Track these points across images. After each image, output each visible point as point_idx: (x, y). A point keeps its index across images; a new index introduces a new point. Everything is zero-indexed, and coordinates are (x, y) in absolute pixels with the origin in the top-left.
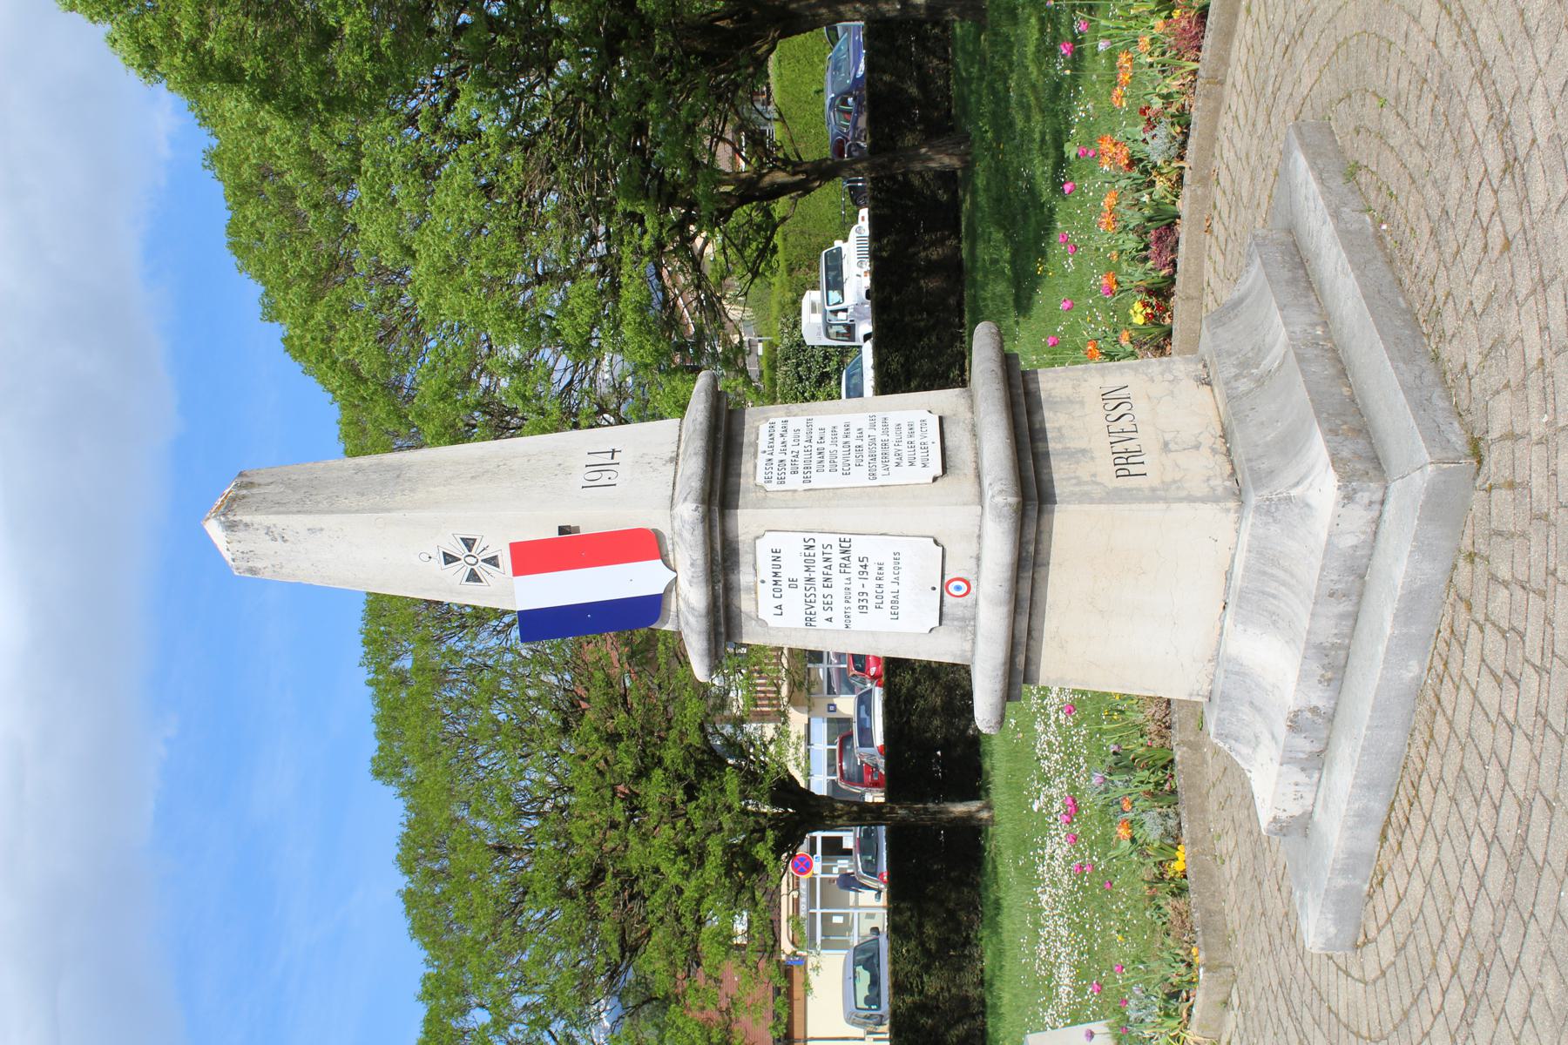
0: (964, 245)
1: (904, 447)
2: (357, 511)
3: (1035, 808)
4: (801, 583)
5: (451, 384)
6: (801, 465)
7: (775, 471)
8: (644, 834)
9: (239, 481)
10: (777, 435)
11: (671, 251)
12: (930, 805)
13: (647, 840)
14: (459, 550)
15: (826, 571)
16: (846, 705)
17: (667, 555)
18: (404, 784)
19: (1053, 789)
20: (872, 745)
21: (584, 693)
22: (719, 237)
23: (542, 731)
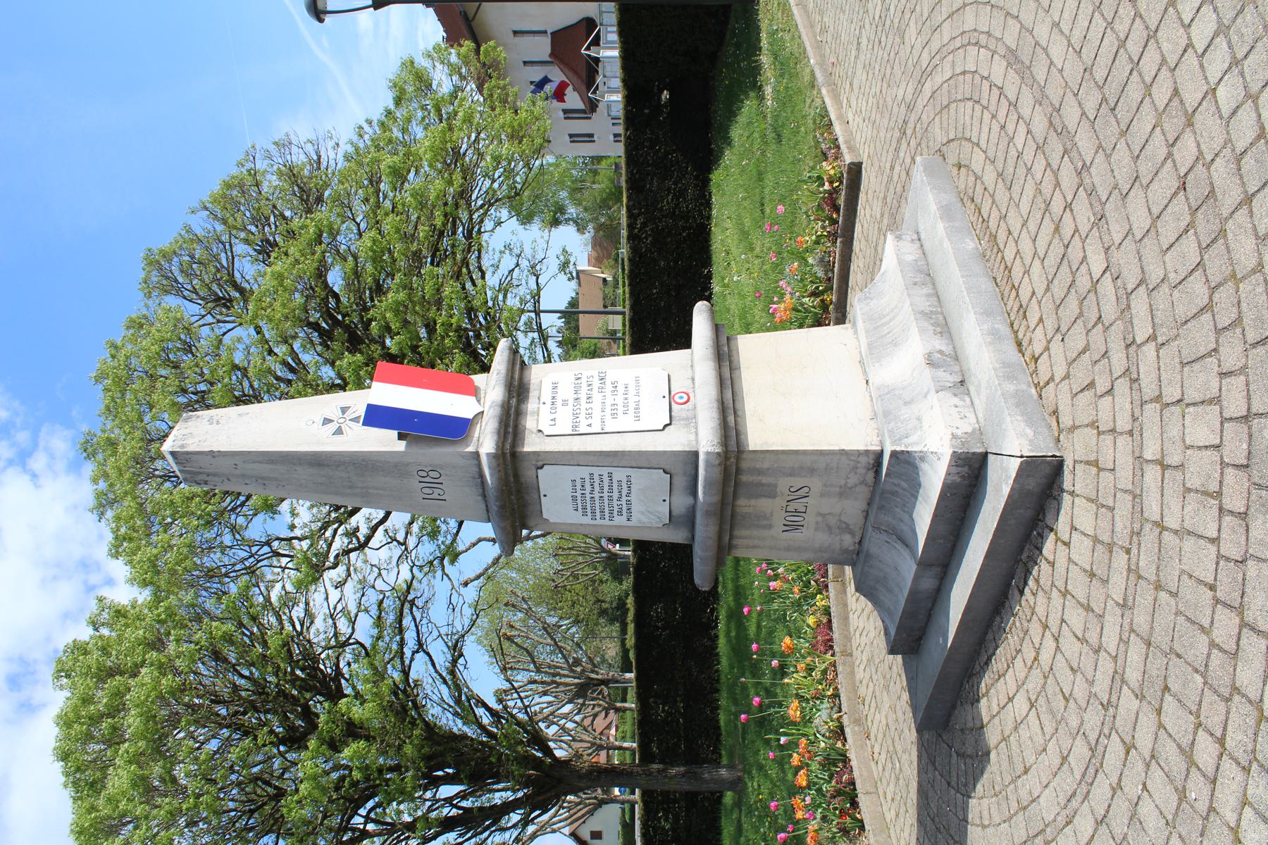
4: (571, 402)
14: (332, 427)
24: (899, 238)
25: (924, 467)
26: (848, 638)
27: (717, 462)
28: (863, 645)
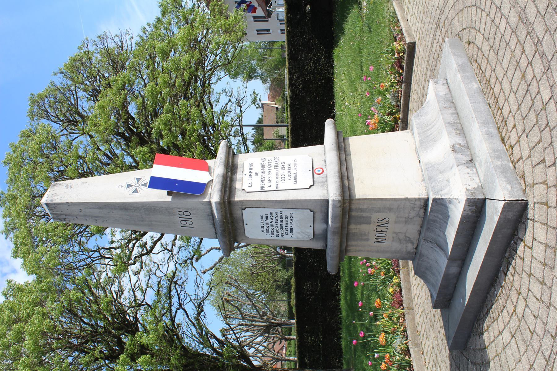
4: (260, 174)
24: (436, 83)
25: (451, 206)
26: (410, 300)
27: (339, 205)
28: (419, 303)
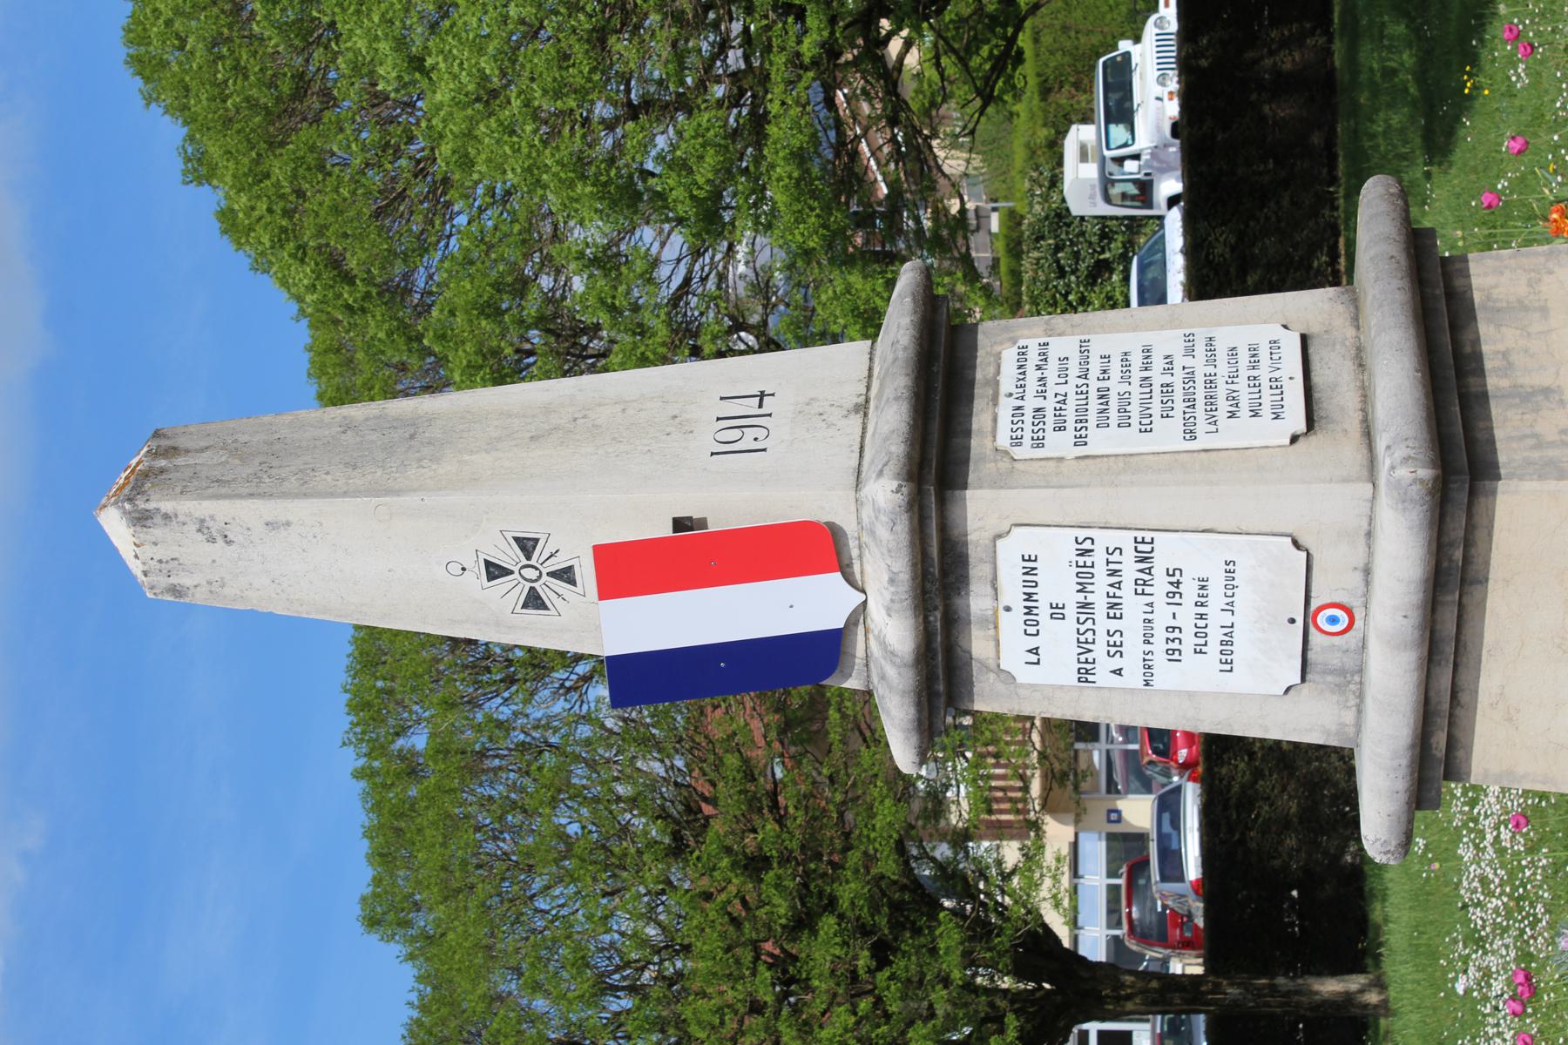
0: (1338, 46)
1: (1242, 385)
2: (345, 494)
3: (1460, 989)
4: (1071, 611)
5: (498, 286)
6: (1070, 416)
7: (1028, 427)
8: (806, 1023)
9: (154, 444)
10: (1030, 367)
11: (847, 63)
12: (1281, 980)
13: (811, 1032)
14: (509, 556)
15: (1112, 591)
16: (1138, 811)
17: (850, 565)
18: (413, 939)
19: (1490, 958)
20: (1180, 878)
21: (707, 790)
22: (929, 38)
23: (640, 852)
